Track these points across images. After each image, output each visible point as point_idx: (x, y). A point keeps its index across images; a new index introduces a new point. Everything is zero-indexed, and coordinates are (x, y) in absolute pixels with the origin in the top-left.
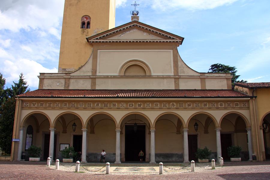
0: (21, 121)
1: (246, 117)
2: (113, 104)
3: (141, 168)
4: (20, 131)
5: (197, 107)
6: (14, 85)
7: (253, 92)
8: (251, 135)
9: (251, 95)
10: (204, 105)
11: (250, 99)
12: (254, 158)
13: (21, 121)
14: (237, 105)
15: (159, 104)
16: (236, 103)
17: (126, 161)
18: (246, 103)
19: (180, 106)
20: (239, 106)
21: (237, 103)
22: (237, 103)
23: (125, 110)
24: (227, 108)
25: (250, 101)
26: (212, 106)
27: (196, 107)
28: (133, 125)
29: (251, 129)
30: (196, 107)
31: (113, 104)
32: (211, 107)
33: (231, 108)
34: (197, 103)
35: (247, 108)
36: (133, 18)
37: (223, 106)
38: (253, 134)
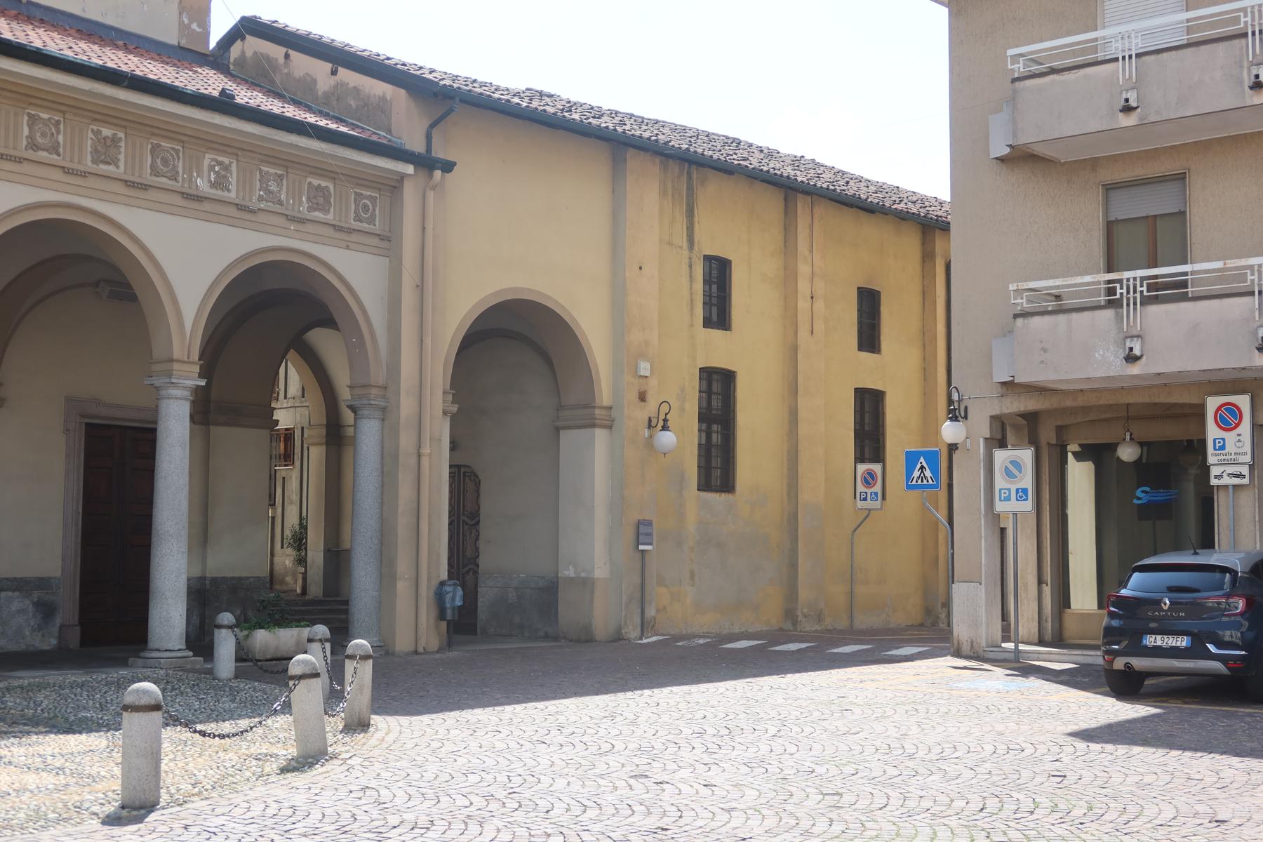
5: (43, 155)
6: (339, 81)
7: (433, 126)
8: (389, 459)
11: (410, 169)
12: (303, 663)
14: (319, 199)
15: (234, 168)
17: (83, 643)
18: (373, 199)
19: (358, 219)
21: (324, 184)
22: (324, 184)
24: (145, 187)
25: (410, 193)
29: (384, 409)
30: (30, 154)
32: (150, 179)
33: (281, 221)
34: (44, 116)
35: (375, 241)
36: (1107, 189)
38: (406, 441)
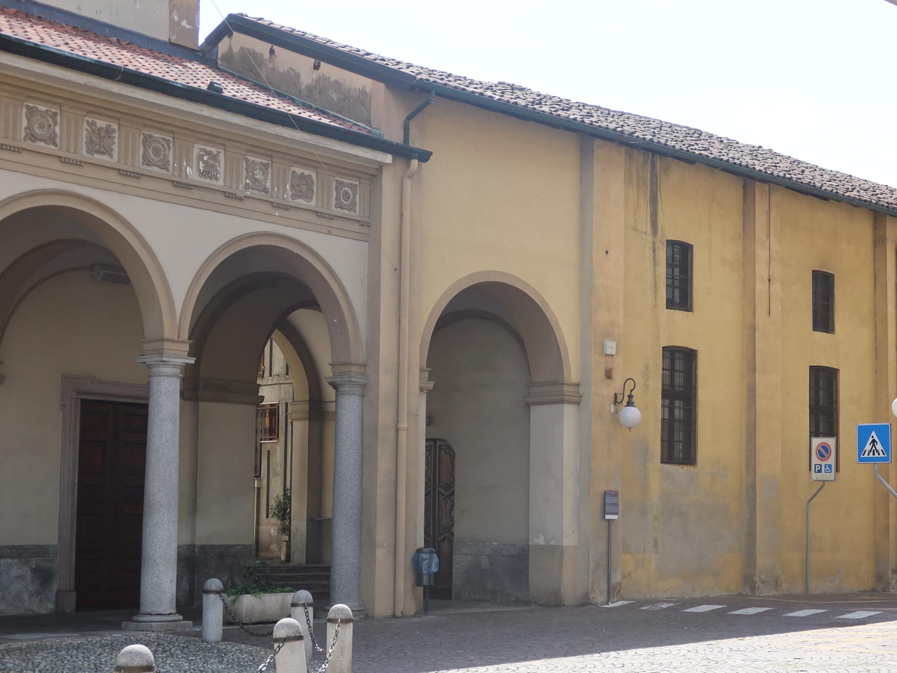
0: (178, 306)
1: (346, 285)
2: (27, 107)
3: (16, 638)
4: (407, 428)
7: (410, 117)
9: (395, 136)
10: (90, 141)
11: (388, 159)
13: (178, 306)
14: (302, 187)
15: (222, 157)
16: (299, 171)
19: (339, 205)
20: (312, 204)
23: (220, 209)
25: (388, 181)
26: (145, 156)
27: (28, 144)
28: (682, 410)
29: (364, 386)
30: (28, 144)
31: (27, 107)
32: (142, 168)
33: (266, 208)
34: (42, 108)
35: (356, 227)
37: (109, 152)
38: (385, 416)
